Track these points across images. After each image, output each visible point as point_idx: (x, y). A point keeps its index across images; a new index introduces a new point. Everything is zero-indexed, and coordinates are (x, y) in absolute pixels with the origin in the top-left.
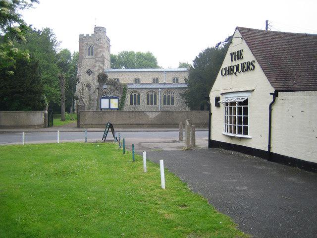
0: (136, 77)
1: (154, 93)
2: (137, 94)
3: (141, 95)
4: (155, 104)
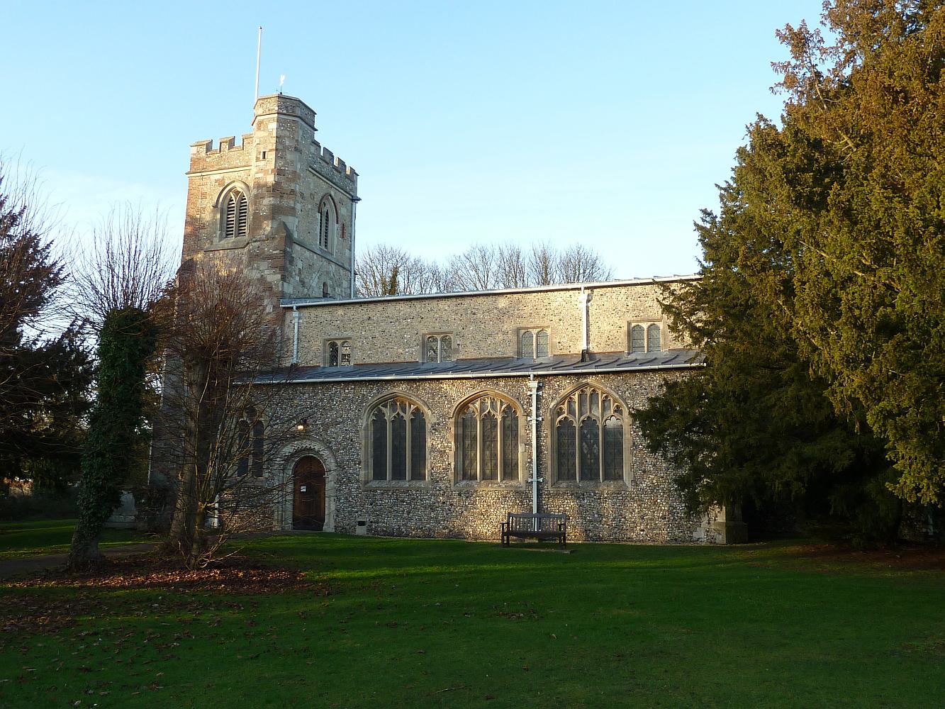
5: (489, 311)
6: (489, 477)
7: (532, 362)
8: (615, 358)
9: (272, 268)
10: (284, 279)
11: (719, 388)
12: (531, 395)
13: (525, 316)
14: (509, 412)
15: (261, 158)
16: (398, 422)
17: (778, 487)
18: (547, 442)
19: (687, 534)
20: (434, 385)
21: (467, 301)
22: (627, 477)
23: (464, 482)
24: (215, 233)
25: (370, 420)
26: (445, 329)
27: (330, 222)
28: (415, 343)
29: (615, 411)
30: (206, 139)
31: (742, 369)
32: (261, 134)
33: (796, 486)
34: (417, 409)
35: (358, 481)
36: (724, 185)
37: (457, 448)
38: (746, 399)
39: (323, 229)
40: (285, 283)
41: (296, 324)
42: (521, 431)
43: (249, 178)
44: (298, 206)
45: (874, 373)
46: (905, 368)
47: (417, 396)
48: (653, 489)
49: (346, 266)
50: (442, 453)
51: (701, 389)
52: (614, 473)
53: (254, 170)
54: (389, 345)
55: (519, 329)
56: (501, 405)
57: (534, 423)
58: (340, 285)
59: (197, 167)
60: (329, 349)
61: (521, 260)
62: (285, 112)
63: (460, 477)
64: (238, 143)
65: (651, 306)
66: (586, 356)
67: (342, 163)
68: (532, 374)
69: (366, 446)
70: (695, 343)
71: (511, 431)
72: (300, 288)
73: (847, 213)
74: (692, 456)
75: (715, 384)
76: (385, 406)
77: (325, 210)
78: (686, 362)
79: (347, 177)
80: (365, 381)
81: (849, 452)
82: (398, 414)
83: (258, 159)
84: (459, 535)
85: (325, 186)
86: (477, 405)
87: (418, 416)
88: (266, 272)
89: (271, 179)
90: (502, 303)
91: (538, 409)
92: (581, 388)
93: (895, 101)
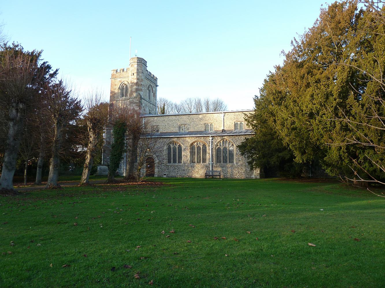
5: (197, 118)
6: (199, 162)
7: (209, 132)
8: (231, 131)
11: (259, 140)
14: (204, 146)
16: (175, 149)
17: (273, 163)
18: (214, 153)
19: (250, 176)
20: (184, 138)
21: (191, 116)
22: (235, 162)
23: (192, 164)
24: (119, 96)
25: (167, 148)
29: (232, 145)
30: (116, 69)
31: (264, 135)
32: (132, 68)
33: (277, 163)
34: (180, 145)
36: (261, 88)
37: (190, 155)
38: (265, 142)
39: (149, 95)
42: (207, 151)
43: (129, 80)
44: (143, 89)
45: (291, 138)
46: (296, 137)
47: (180, 141)
48: (241, 165)
49: (155, 105)
50: (186, 156)
51: (255, 140)
52: (231, 161)
53: (130, 78)
55: (205, 123)
56: (202, 144)
57: (211, 148)
59: (113, 77)
61: (201, 102)
63: (191, 162)
64: (125, 70)
65: (241, 118)
66: (223, 131)
67: (153, 76)
68: (210, 136)
70: (253, 129)
71: (205, 151)
73: (286, 107)
74: (252, 156)
75: (258, 139)
76: (171, 144)
78: (250, 133)
79: (155, 79)
80: (165, 137)
81: (289, 155)
82: (174, 146)
83: (131, 75)
84: (191, 177)
86: (196, 143)
87: (180, 146)
89: (135, 81)
90: (201, 116)
91: (212, 145)
92: (223, 139)
93: (295, 85)
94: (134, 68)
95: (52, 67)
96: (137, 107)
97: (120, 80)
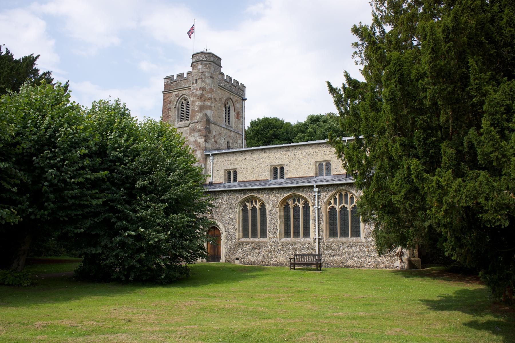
0: (229, 167)
1: (302, 202)
2: (258, 207)
3: (268, 207)
4: (307, 234)
9: (200, 135)
10: (206, 141)
12: (315, 196)
13: (319, 155)
15: (195, 83)
24: (175, 120)
26: (281, 163)
27: (231, 112)
28: (267, 170)
35: (235, 239)
37: (281, 222)
40: (206, 143)
41: (212, 163)
44: (213, 105)
54: (255, 172)
58: (237, 142)
60: (227, 174)
62: (205, 60)
69: (239, 221)
72: (215, 145)
76: (248, 202)
77: (228, 106)
82: (254, 206)
85: (227, 94)
88: (198, 138)
91: (318, 202)
94: (197, 71)
95: (53, 79)
96: (201, 138)
97: (176, 93)
